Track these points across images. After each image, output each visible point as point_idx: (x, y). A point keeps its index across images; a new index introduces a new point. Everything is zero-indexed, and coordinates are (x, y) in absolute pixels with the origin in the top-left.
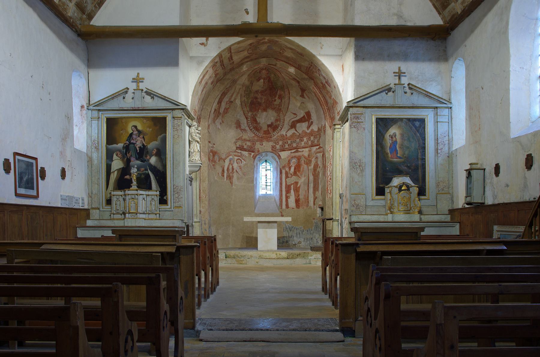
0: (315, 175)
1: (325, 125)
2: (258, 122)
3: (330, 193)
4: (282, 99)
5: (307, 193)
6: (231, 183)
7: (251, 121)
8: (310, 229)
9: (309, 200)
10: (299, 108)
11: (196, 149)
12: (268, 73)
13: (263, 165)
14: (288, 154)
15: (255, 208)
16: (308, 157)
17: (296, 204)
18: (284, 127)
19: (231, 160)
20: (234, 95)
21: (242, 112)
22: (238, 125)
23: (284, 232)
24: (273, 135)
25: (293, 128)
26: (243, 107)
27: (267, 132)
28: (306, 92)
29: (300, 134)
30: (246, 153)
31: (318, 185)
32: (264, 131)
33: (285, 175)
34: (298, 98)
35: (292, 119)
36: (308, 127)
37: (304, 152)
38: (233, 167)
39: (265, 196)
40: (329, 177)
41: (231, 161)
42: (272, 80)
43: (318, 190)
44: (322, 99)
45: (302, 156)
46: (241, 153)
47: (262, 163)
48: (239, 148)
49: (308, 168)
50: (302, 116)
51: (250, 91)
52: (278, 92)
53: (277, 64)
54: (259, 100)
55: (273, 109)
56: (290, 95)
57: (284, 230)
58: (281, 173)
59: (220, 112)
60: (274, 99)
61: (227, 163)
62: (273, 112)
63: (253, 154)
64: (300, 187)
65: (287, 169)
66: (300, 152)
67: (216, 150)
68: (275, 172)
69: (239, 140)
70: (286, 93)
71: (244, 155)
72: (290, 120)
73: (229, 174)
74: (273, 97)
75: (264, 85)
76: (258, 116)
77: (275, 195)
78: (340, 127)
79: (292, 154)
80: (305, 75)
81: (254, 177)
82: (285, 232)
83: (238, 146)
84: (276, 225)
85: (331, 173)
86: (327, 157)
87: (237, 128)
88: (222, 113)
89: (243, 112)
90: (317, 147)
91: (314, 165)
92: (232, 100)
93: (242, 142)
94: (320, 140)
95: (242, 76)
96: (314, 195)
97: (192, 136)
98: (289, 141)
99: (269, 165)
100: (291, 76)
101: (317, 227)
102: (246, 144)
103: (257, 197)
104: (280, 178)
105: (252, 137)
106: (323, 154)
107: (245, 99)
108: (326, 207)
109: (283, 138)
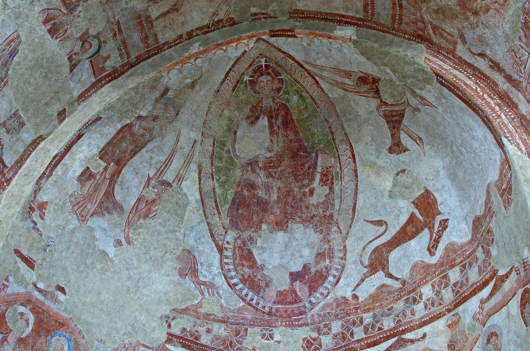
2: (259, 263)
4: (332, 183)
7: (234, 259)
10: (392, 195)
12: (279, 90)
18: (347, 271)
20: (175, 161)
24: (308, 305)
25: (378, 271)
26: (208, 214)
28: (405, 121)
29: (404, 283)
32: (279, 293)
35: (371, 242)
37: (427, 340)
42: (294, 117)
48: (180, 338)
50: (404, 219)
51: (231, 158)
52: (319, 164)
54: (260, 193)
55: (308, 220)
56: (355, 162)
59: (118, 198)
60: (307, 190)
62: (308, 231)
66: (412, 341)
67: (64, 315)
69: (187, 314)
70: (343, 159)
72: (364, 249)
74: (306, 182)
75: (271, 141)
76: (259, 243)
83: (176, 330)
87: (182, 274)
89: (207, 227)
90: (485, 292)
92: (169, 176)
93: (195, 322)
95: (193, 86)
98: (365, 315)
102: (209, 331)
107: (216, 185)
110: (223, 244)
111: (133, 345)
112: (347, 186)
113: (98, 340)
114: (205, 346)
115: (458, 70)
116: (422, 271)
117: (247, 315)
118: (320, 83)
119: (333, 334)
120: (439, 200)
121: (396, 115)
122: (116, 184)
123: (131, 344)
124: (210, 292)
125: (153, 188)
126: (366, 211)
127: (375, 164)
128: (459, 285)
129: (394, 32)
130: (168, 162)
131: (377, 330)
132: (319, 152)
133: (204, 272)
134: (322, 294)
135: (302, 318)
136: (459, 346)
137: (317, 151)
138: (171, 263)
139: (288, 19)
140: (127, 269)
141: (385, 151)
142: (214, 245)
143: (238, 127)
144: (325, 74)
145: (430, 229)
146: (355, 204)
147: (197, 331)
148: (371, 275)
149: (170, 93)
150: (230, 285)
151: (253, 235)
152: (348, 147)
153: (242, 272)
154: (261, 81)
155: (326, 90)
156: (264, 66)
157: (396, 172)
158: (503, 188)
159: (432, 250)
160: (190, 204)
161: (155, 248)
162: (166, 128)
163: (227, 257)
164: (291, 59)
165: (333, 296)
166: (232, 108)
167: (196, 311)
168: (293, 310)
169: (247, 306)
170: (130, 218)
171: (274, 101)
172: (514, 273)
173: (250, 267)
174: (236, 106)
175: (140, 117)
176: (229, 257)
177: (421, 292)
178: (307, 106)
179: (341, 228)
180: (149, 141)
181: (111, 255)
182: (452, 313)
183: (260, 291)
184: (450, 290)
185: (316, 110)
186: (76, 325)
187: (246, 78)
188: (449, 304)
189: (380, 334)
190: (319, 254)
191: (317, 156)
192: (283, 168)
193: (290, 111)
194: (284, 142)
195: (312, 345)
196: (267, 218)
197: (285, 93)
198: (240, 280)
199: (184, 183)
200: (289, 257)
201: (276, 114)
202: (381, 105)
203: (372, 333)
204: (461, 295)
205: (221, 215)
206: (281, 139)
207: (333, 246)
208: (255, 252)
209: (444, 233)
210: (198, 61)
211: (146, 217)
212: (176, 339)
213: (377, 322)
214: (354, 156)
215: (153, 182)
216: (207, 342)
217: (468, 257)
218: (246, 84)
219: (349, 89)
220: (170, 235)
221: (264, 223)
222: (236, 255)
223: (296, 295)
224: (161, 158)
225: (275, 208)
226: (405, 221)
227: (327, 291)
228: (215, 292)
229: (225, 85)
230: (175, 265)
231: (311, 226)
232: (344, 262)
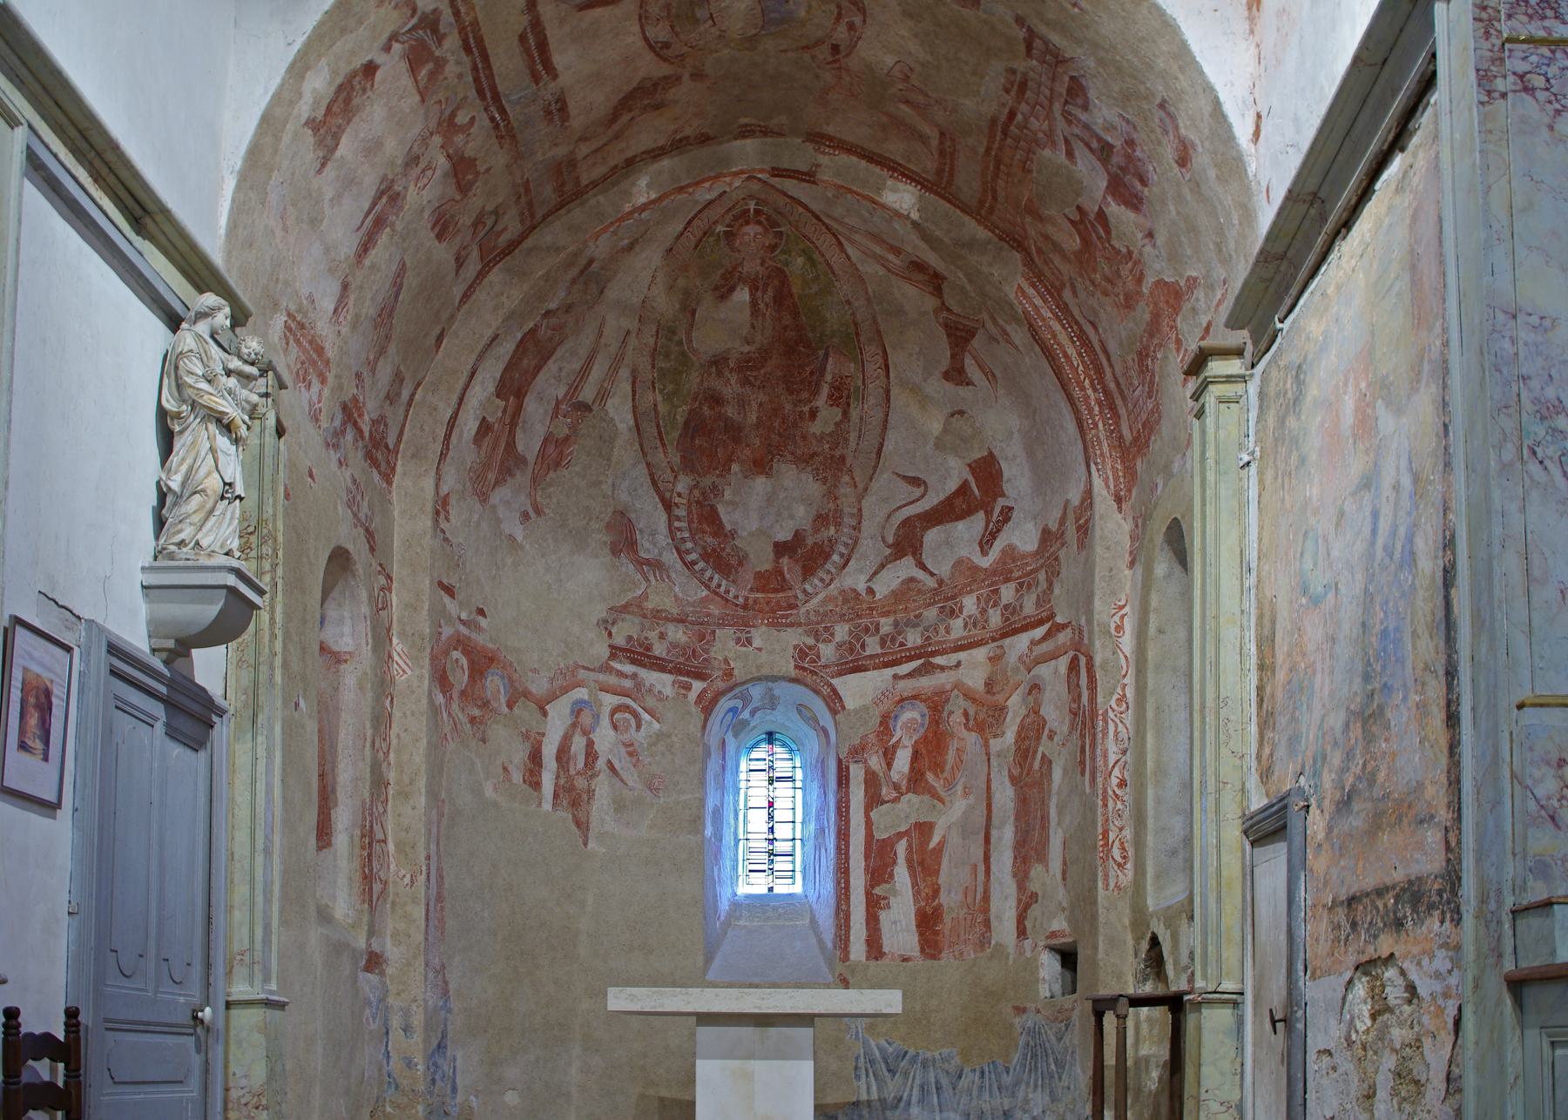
0: (1028, 780)
1: (1088, 494)
2: (728, 527)
3: (1119, 860)
4: (849, 405)
5: (981, 876)
6: (582, 825)
7: (690, 522)
8: (999, 1062)
9: (993, 910)
10: (939, 445)
11: (209, 474)
13: (754, 755)
14: (878, 684)
15: (709, 960)
16: (988, 692)
17: (921, 934)
19: (581, 710)
20: (596, 367)
21: (641, 471)
22: (624, 539)
23: (858, 1077)
24: (801, 596)
27: (771, 581)
28: (976, 343)
29: (941, 582)
30: (662, 682)
31: (1045, 827)
32: (759, 576)
34: (936, 386)
35: (900, 507)
36: (985, 544)
37: (961, 670)
38: (590, 744)
39: (766, 904)
40: (1116, 772)
42: (795, 290)
43: (1042, 857)
44: (1071, 351)
46: (634, 676)
49: (986, 745)
50: (952, 485)
51: (683, 354)
52: (829, 368)
53: (818, 166)
54: (730, 411)
55: (804, 460)
57: (856, 1068)
58: (843, 779)
59: (520, 448)
60: (806, 409)
62: (803, 476)
63: (698, 686)
64: (941, 851)
65: (875, 762)
66: (943, 668)
67: (491, 646)
69: (629, 613)
71: (650, 690)
72: (889, 517)
73: (570, 779)
74: (805, 395)
75: (753, 327)
76: (728, 495)
77: (812, 897)
78: (1242, 371)
79: (902, 684)
80: (973, 223)
82: (864, 1077)
83: (620, 641)
84: (805, 1034)
85: (1124, 752)
86: (1105, 663)
87: (615, 552)
89: (646, 471)
90: (1039, 632)
91: (1022, 727)
92: (587, 394)
93: (642, 624)
94: (1052, 592)
95: (630, 247)
96: (1021, 887)
97: (180, 386)
98: (883, 620)
100: (897, 251)
101: (1034, 1056)
102: (662, 636)
103: (724, 906)
104: (839, 808)
106: (1073, 666)
107: (659, 399)
108: (1101, 938)
109: (855, 605)
112: (872, 414)
114: (660, 659)
115: (1060, 321)
116: (967, 573)
128: (1011, 609)
133: (647, 545)
138: (599, 536)
142: (657, 499)
143: (698, 303)
144: (857, 237)
145: (986, 512)
146: (882, 445)
147: (646, 638)
149: (594, 265)
150: (685, 564)
151: (717, 481)
154: (745, 234)
155: (854, 259)
157: (950, 411)
158: (1130, 264)
163: (678, 519)
167: (639, 606)
169: (712, 596)
171: (762, 264)
172: (1069, 630)
173: (715, 535)
175: (548, 313)
182: (995, 644)
183: (730, 572)
184: (999, 612)
187: (720, 228)
189: (901, 651)
190: (819, 516)
191: (826, 356)
192: (769, 369)
195: (807, 655)
197: (784, 252)
199: (610, 402)
204: (1010, 624)
208: (721, 509)
213: (899, 633)
214: (887, 367)
217: (1029, 574)
226: (953, 489)
227: (829, 577)
229: (683, 239)
230: (604, 539)
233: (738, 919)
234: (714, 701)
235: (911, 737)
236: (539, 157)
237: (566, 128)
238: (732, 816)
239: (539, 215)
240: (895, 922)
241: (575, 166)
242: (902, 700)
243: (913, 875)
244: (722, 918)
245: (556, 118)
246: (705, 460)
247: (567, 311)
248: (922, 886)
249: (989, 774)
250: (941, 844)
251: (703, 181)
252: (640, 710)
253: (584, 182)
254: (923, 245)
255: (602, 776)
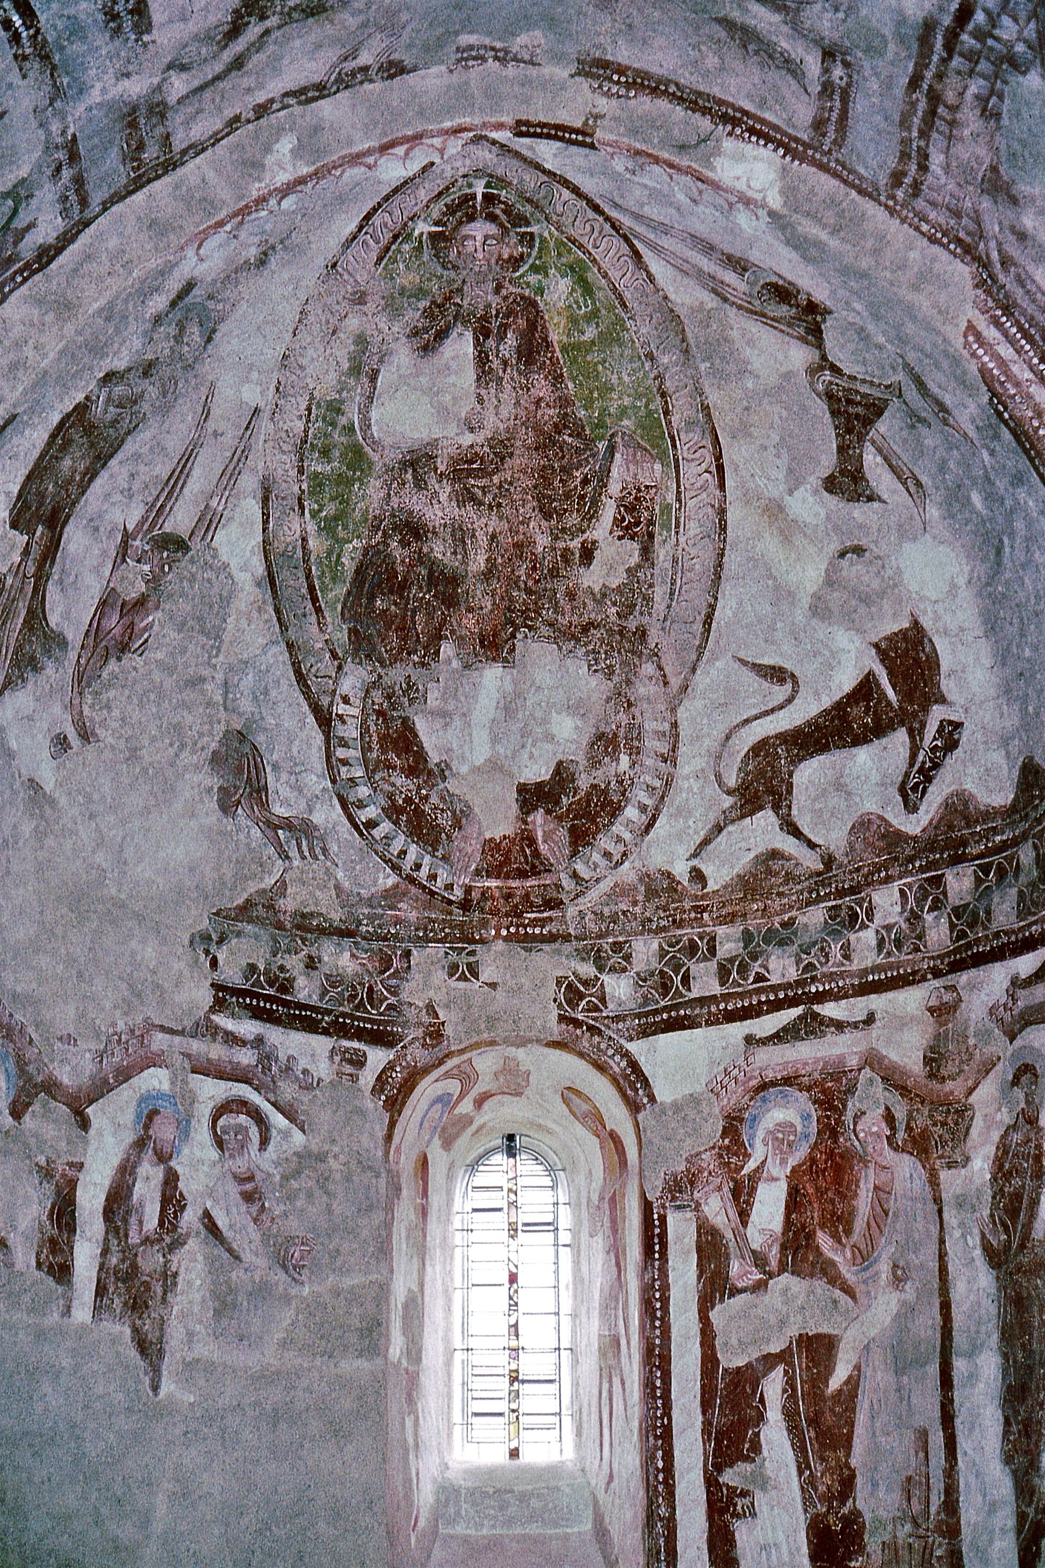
2: (434, 757)
4: (651, 536)
7: (366, 749)
10: (819, 609)
12: (517, 262)
13: (479, 1180)
16: (931, 1076)
18: (677, 798)
20: (196, 472)
24: (567, 883)
25: (761, 808)
26: (287, 615)
28: (882, 426)
29: (829, 861)
32: (491, 846)
33: (700, 1265)
35: (747, 721)
38: (171, 1179)
41: (157, 1120)
45: (867, 1073)
46: (259, 1041)
47: (473, 1167)
49: (934, 1181)
50: (846, 681)
52: (615, 473)
54: (439, 550)
56: (722, 486)
59: (54, 619)
60: (575, 544)
61: (109, 1140)
63: (377, 1057)
66: (840, 1026)
68: (598, 1246)
70: (690, 472)
71: (288, 1069)
72: (728, 738)
73: (129, 1254)
74: (573, 520)
75: (480, 400)
80: (881, 214)
81: (383, 1290)
83: (232, 974)
87: (227, 805)
88: (74, 635)
91: (1003, 1148)
98: (721, 931)
99: (547, 1181)
102: (311, 964)
103: (425, 1496)
105: (370, 903)
107: (311, 527)
110: (331, 704)
111: (137, 1033)
112: (693, 552)
113: (61, 1039)
117: (405, 911)
118: (645, 259)
119: (638, 974)
120: (946, 663)
121: (860, 403)
122: (50, 582)
123: (132, 1031)
124: (305, 848)
125: (139, 561)
126: (741, 633)
127: (781, 508)
129: (891, 203)
130: (178, 478)
131: (751, 979)
132: (618, 439)
133: (285, 792)
134: (607, 855)
135: (550, 919)
136: (949, 1068)
137: (612, 436)
139: (572, 76)
140: (91, 817)
141: (814, 480)
142: (306, 708)
143: (381, 361)
144: (666, 242)
145: (911, 732)
146: (712, 607)
147: (282, 968)
148: (743, 817)
149: (196, 291)
150: (356, 826)
151: (415, 674)
152: (708, 442)
153: (387, 787)
154: (466, 237)
156: (479, 197)
159: (912, 796)
160: (240, 595)
161: (153, 740)
162: (176, 384)
163: (344, 743)
164: (568, 188)
165: (638, 864)
166: (370, 307)
167: (270, 907)
168: (527, 895)
170: (82, 661)
171: (498, 290)
173: (411, 772)
174: (383, 302)
176: (351, 743)
177: (870, 901)
178: (599, 310)
179: (668, 669)
180: (129, 433)
181: (49, 786)
185: (622, 326)
186: (11, 1015)
187: (422, 228)
188: (939, 956)
189: (758, 991)
190: (600, 736)
191: (611, 450)
193: (542, 318)
194: (518, 403)
195: (582, 996)
196: (455, 623)
197: (535, 269)
198: (383, 809)
200: (515, 738)
201: (502, 325)
202: (822, 368)
203: (739, 985)
204: (969, 946)
205: (324, 618)
206: (507, 395)
207: (640, 720)
208: (421, 725)
209: (948, 760)
210: (286, 204)
211: (123, 651)
212: (234, 999)
213: (754, 958)
214: (720, 468)
215: (137, 543)
216: (310, 996)
218: (421, 242)
219: (732, 299)
220: (189, 695)
221: (447, 638)
222: (370, 736)
223: (536, 854)
224: (157, 471)
225: (478, 592)
227: (621, 848)
228: (318, 850)
231: (581, 652)
232: (673, 770)
233: (451, 1522)
234: (408, 1086)
235: (783, 1162)
236: (95, 96)
237: (145, 45)
238: (440, 1302)
239: (96, 199)
240: (764, 1547)
241: (163, 116)
242: (763, 1086)
243: (800, 1449)
244: (422, 1523)
245: (127, 25)
246: (393, 635)
247: (146, 374)
248: (818, 1468)
249: (942, 1242)
250: (853, 1383)
251: (392, 144)
252: (266, 1107)
253: (179, 143)
254: (787, 253)
255: (192, 1244)
